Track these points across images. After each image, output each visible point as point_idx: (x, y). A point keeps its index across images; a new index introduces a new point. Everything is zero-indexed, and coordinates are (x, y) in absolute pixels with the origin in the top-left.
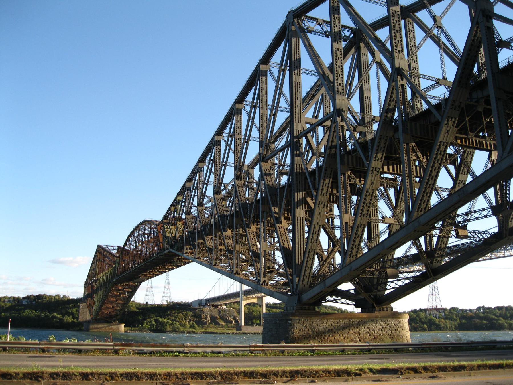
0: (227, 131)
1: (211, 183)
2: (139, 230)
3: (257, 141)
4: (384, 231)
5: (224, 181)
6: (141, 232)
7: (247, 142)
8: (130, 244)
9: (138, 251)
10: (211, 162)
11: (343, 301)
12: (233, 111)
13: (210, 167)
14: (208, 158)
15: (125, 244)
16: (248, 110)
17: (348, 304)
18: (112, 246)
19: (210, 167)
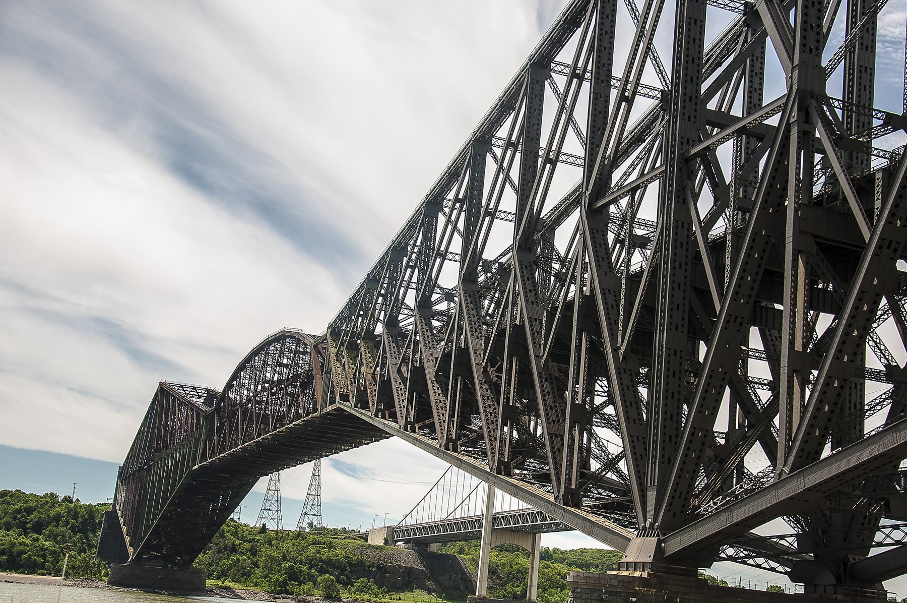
0: (503, 132)
1: (500, 143)
2: (267, 353)
3: (578, 165)
4: (881, 403)
5: (484, 256)
6: (270, 359)
7: (554, 163)
8: (242, 386)
9: (260, 402)
10: (458, 205)
11: (760, 560)
12: (521, 86)
13: (453, 218)
14: (451, 196)
15: (229, 386)
16: (562, 88)
17: (773, 569)
18: (194, 388)
19: (453, 218)
